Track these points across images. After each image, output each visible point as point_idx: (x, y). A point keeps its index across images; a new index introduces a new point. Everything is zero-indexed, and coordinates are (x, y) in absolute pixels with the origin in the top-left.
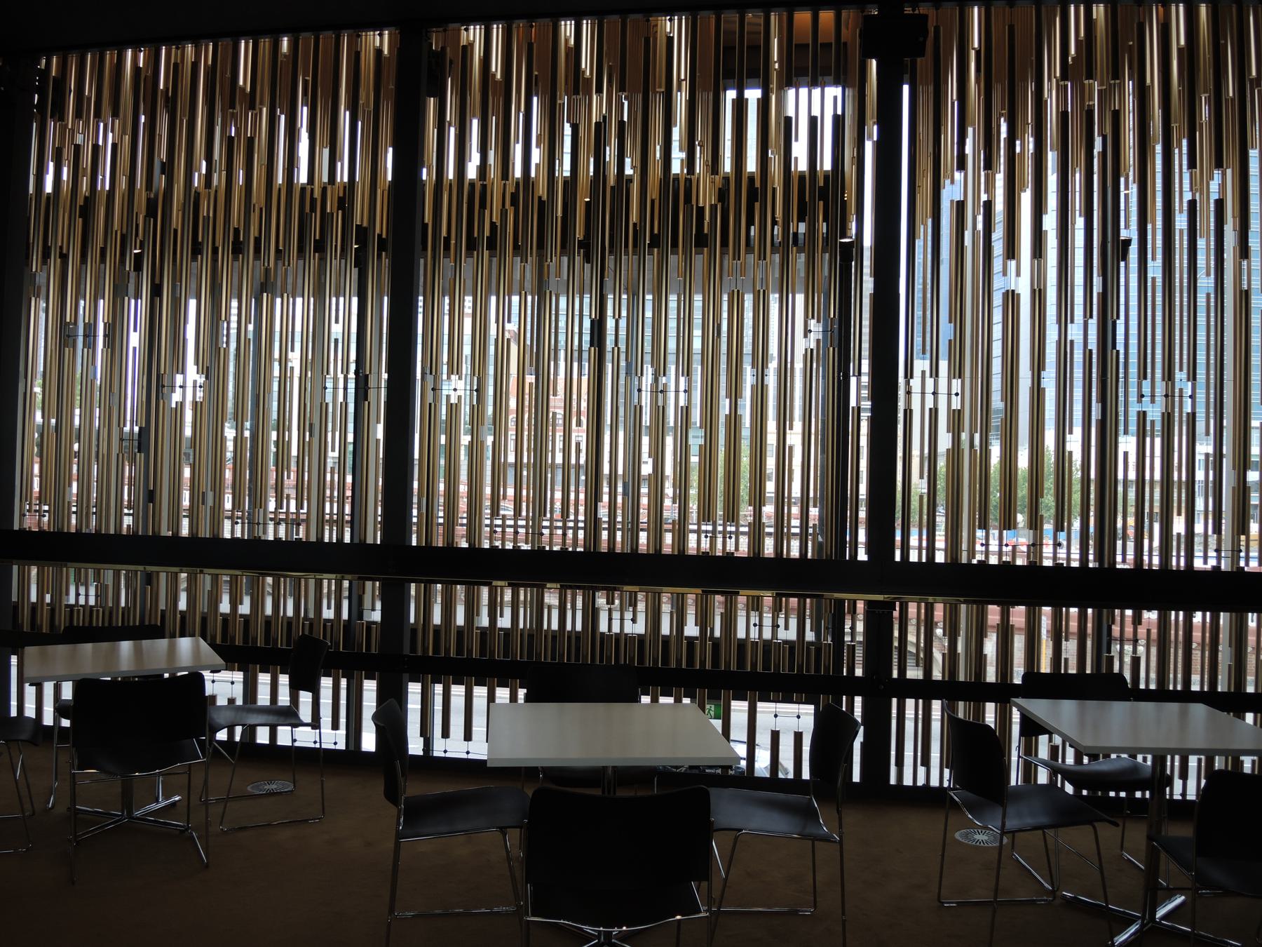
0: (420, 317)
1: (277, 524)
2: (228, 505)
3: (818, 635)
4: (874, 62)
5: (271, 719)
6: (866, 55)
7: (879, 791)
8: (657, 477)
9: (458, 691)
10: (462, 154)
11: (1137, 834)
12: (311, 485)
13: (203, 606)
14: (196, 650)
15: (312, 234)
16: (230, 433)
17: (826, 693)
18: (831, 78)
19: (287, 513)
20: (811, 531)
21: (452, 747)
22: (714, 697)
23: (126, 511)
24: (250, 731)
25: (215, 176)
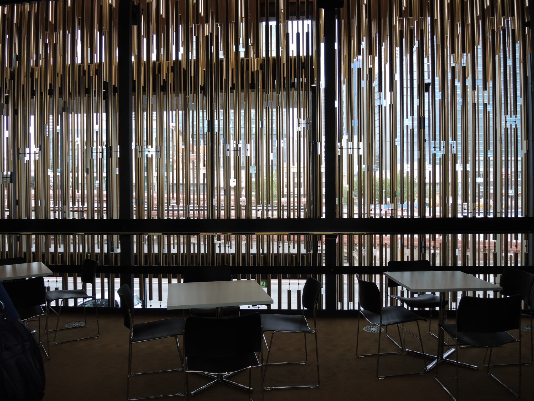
0: (133, 122)
1: (55, 212)
2: (52, 206)
3: (307, 251)
4: (323, 10)
5: (74, 296)
6: (320, 6)
7: (334, 313)
8: (238, 189)
9: (155, 281)
10: (149, 51)
11: (435, 325)
12: (88, 195)
13: (43, 249)
14: (40, 268)
15: (77, 87)
16: (51, 173)
17: (310, 274)
18: (305, 17)
19: (78, 207)
20: (302, 208)
21: (154, 304)
22: (264, 278)
23: (7, 209)
24: (66, 301)
25: (40, 61)
